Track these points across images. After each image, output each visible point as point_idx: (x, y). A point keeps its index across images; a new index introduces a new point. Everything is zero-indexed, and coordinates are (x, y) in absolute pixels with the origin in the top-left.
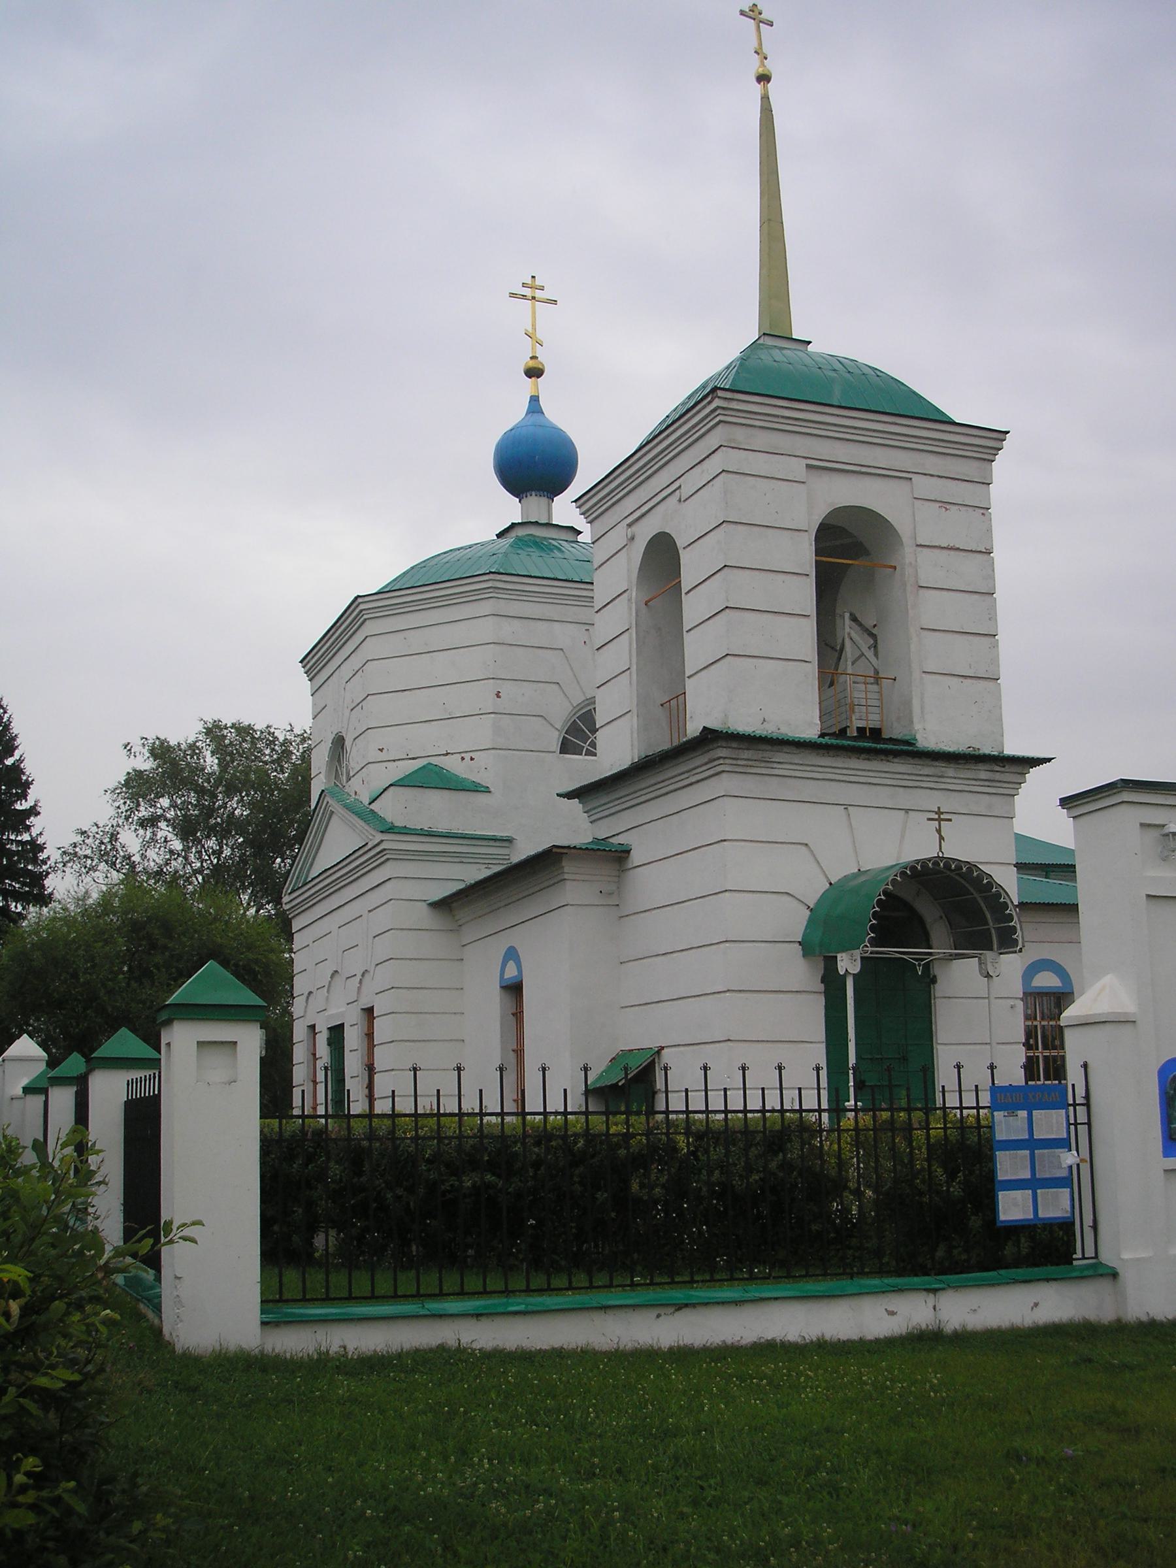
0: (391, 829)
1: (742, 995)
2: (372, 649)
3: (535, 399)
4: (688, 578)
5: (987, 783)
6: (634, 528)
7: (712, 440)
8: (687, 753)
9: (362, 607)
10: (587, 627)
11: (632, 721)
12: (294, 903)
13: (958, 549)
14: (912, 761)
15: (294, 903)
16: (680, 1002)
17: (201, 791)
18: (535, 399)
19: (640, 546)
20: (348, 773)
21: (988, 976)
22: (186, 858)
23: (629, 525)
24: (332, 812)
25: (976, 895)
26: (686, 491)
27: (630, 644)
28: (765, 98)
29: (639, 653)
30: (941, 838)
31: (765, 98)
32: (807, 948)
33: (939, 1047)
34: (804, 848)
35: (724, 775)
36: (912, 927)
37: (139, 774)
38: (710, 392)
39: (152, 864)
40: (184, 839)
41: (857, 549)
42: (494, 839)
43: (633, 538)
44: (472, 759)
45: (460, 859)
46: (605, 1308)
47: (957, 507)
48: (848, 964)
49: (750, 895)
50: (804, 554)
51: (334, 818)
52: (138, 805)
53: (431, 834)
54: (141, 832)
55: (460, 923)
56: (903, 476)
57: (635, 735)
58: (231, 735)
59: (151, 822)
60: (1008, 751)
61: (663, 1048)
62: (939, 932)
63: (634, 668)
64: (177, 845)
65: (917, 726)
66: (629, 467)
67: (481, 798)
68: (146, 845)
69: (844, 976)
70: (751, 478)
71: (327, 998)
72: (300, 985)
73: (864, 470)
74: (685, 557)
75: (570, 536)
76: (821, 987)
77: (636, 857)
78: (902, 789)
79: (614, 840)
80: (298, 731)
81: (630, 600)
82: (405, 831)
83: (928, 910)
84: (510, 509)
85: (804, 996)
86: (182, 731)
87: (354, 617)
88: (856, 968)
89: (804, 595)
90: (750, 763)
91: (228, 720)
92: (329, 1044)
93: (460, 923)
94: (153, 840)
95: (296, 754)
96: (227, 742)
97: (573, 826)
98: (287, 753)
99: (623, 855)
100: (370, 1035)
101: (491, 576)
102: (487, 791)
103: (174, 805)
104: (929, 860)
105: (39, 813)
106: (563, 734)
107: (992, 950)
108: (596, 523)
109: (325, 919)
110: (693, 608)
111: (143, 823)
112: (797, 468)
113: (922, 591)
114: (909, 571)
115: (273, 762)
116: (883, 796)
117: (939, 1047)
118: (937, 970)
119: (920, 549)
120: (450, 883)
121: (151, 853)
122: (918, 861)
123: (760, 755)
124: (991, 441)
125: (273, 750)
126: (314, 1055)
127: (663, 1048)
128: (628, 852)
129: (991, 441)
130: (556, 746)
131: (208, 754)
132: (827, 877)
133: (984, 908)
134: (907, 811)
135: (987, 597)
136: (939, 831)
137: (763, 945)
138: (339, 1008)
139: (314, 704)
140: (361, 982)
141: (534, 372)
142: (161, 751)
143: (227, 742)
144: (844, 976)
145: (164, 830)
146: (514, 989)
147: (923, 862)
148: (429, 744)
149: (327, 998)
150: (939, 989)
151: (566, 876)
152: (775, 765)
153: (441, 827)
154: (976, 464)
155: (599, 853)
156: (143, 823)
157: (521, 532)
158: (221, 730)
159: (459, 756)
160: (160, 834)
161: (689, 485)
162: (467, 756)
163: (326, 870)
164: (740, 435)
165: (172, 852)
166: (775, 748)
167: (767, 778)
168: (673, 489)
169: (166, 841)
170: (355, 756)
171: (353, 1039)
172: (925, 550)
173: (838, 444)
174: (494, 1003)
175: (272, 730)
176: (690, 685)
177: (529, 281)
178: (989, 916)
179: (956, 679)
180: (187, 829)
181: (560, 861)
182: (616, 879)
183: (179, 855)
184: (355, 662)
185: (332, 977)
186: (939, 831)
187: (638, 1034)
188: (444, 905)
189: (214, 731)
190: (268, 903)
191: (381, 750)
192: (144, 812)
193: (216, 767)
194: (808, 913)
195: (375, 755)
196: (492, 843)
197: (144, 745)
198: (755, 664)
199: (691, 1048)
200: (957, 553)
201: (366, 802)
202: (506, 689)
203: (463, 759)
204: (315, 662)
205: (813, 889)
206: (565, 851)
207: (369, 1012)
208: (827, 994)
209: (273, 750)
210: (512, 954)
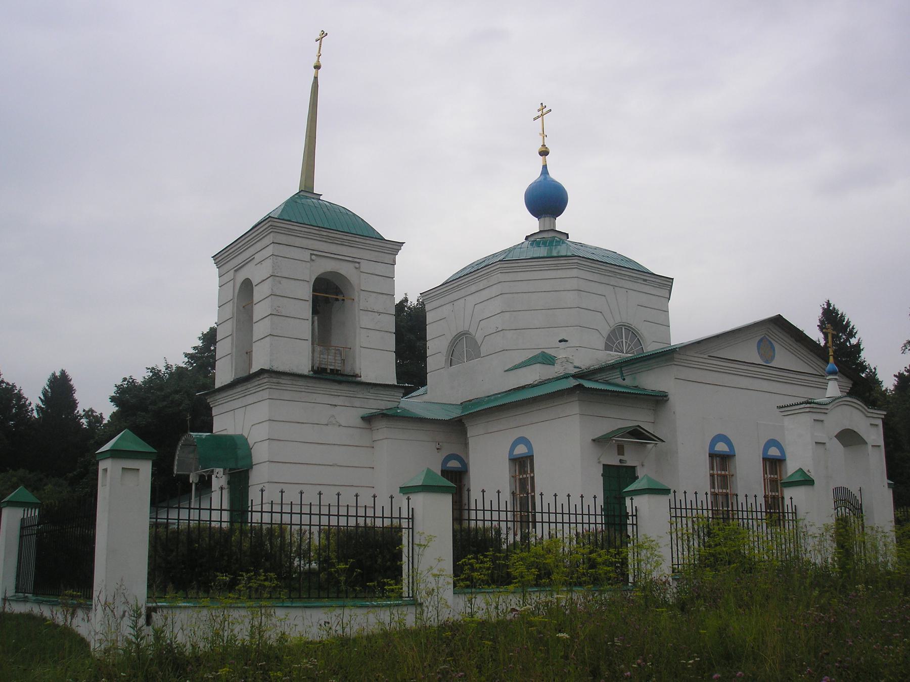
4: (256, 298)
28: (316, 78)
31: (316, 78)
38: (269, 218)
41: (337, 291)
46: (378, 606)
50: (306, 292)
74: (256, 289)
75: (564, 237)
84: (533, 225)
105: (63, 373)
112: (306, 255)
161: (258, 258)
176: (255, 347)
188: (368, 419)
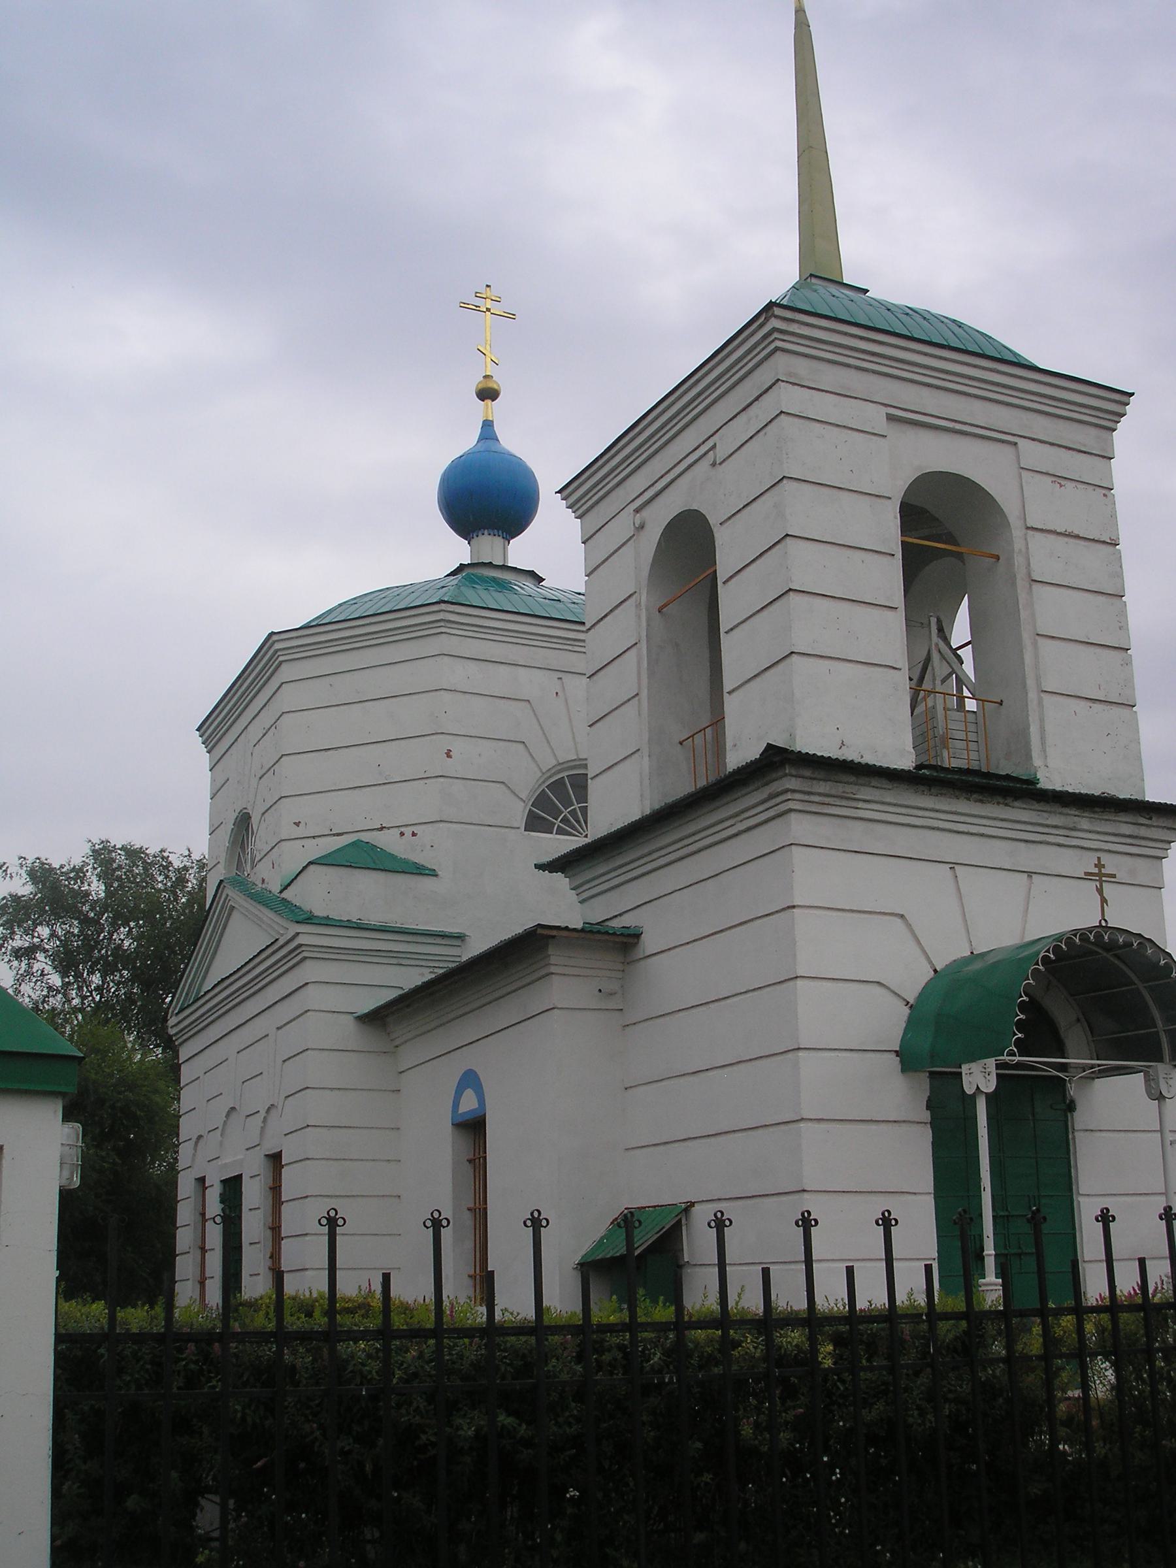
0: (310, 919)
1: (823, 1126)
2: (289, 698)
3: (488, 425)
4: (725, 564)
5: (1129, 841)
6: (645, 513)
7: (763, 377)
8: (738, 788)
9: (277, 646)
10: (560, 675)
11: (643, 763)
12: (182, 1026)
13: (1077, 537)
14: (1037, 806)
15: (182, 1026)
16: (720, 1139)
17: (85, 921)
18: (488, 425)
19: (654, 533)
20: (253, 861)
21: (1161, 1098)
22: (65, 995)
23: (637, 511)
24: (233, 908)
25: (1141, 986)
26: (721, 453)
27: (639, 663)
29: (651, 674)
30: (1104, 901)
32: (908, 1059)
33: (1081, 1199)
34: (899, 920)
35: (793, 815)
36: (1028, 1040)
37: (16, 898)
39: (27, 1000)
40: (64, 974)
42: (443, 936)
43: (642, 527)
44: (414, 834)
45: (397, 959)
47: (1074, 484)
48: (980, 1078)
49: (829, 984)
50: (887, 529)
51: (235, 914)
52: (13, 933)
53: (360, 927)
54: (16, 963)
55: (397, 1042)
56: (1007, 440)
57: (646, 782)
58: (121, 859)
59: (27, 953)
60: (1151, 797)
61: (693, 1204)
62: (1075, 1037)
63: (644, 694)
64: (56, 980)
65: (1037, 762)
66: (640, 433)
67: (427, 883)
68: (20, 980)
69: (974, 1096)
70: (818, 425)
71: (221, 1144)
72: (187, 1128)
73: (958, 427)
74: (722, 537)
76: (926, 1116)
77: (649, 943)
78: (1023, 845)
79: (616, 924)
80: (196, 856)
81: (638, 606)
82: (327, 922)
83: (1063, 1013)
85: (904, 1127)
86: (67, 851)
87: (271, 656)
88: (990, 1086)
89: (887, 580)
90: (827, 800)
91: (118, 841)
92: (221, 1202)
93: (397, 1042)
94: (29, 973)
95: (192, 883)
96: (115, 865)
97: (560, 904)
98: (181, 881)
99: (631, 940)
100: (276, 1189)
101: (443, 606)
102: (433, 874)
103: (53, 935)
104: (1090, 929)
106: (529, 806)
107: (1160, 1059)
108: (588, 517)
109: (221, 1043)
110: (733, 603)
111: (18, 954)
112: (875, 417)
113: (1035, 586)
114: (1019, 561)
115: (165, 890)
116: (999, 852)
117: (1081, 1199)
118: (1072, 1090)
119: (1030, 532)
120: (384, 990)
121: (26, 988)
122: (1075, 932)
123: (839, 789)
124: (1105, 405)
125: (167, 877)
126: (203, 1214)
127: (693, 1204)
128: (638, 936)
129: (1105, 405)
130: (520, 820)
131: (94, 879)
132: (930, 962)
133: (1151, 1003)
134: (1030, 874)
135: (1115, 600)
136: (1100, 891)
137: (848, 1054)
138: (238, 1154)
139: (213, 780)
140: (265, 1120)
141: (487, 394)
142: (41, 874)
143: (115, 865)
144: (974, 1096)
145: (42, 963)
146: (474, 1128)
147: (1083, 934)
148: (357, 815)
149: (221, 1144)
150: (1080, 1119)
151: (553, 969)
152: (860, 805)
153: (374, 919)
154: (1093, 431)
155: (598, 937)
156: (18, 954)
157: (471, 571)
158: (110, 852)
159: (397, 832)
160: (37, 966)
161: (725, 443)
162: (408, 831)
163: (223, 980)
164: (802, 368)
165: (50, 988)
166: (862, 780)
167: (850, 823)
168: (705, 452)
169: (42, 975)
170: (261, 840)
171: (253, 1194)
172: (1038, 535)
173: (925, 391)
174: (442, 1148)
175: (165, 854)
177: (482, 289)
178: (1156, 1014)
179: (1083, 703)
180: (66, 962)
181: (545, 947)
182: (620, 975)
183: (58, 992)
184: (266, 719)
185: (228, 1115)
186: (1100, 891)
187: (651, 1186)
188: (377, 1019)
189: (102, 855)
190: (157, 1046)
191: (297, 824)
192: (19, 942)
193: (103, 895)
194: (907, 1011)
195: (288, 831)
196: (439, 941)
197: (21, 865)
198: (832, 669)
199: (740, 1203)
200: (1078, 541)
201: (276, 889)
202: (457, 746)
203: (402, 834)
204: (216, 728)
205: (913, 978)
206: (554, 933)
207: (275, 1159)
208: (936, 1125)
209: (167, 877)
210: (470, 1080)
